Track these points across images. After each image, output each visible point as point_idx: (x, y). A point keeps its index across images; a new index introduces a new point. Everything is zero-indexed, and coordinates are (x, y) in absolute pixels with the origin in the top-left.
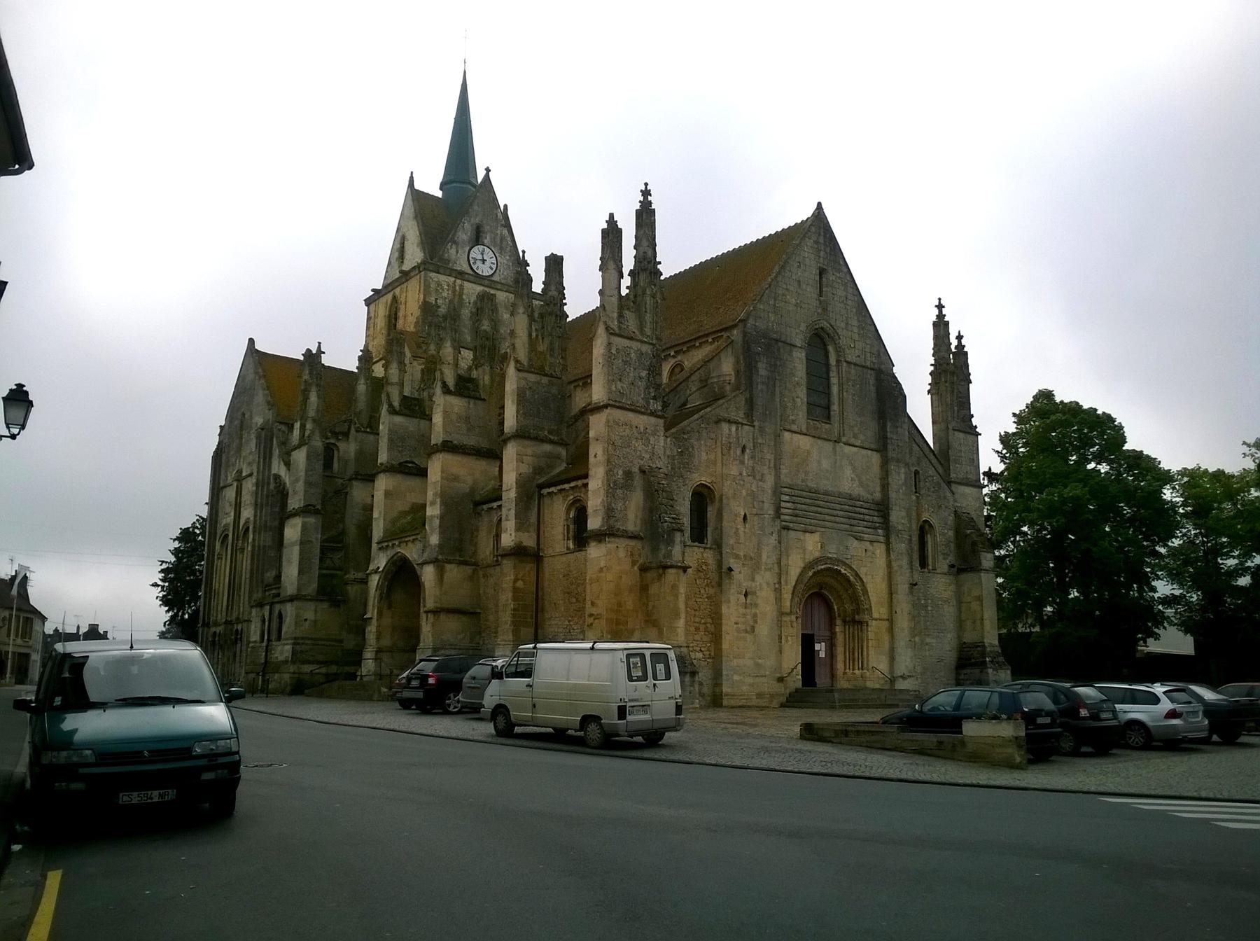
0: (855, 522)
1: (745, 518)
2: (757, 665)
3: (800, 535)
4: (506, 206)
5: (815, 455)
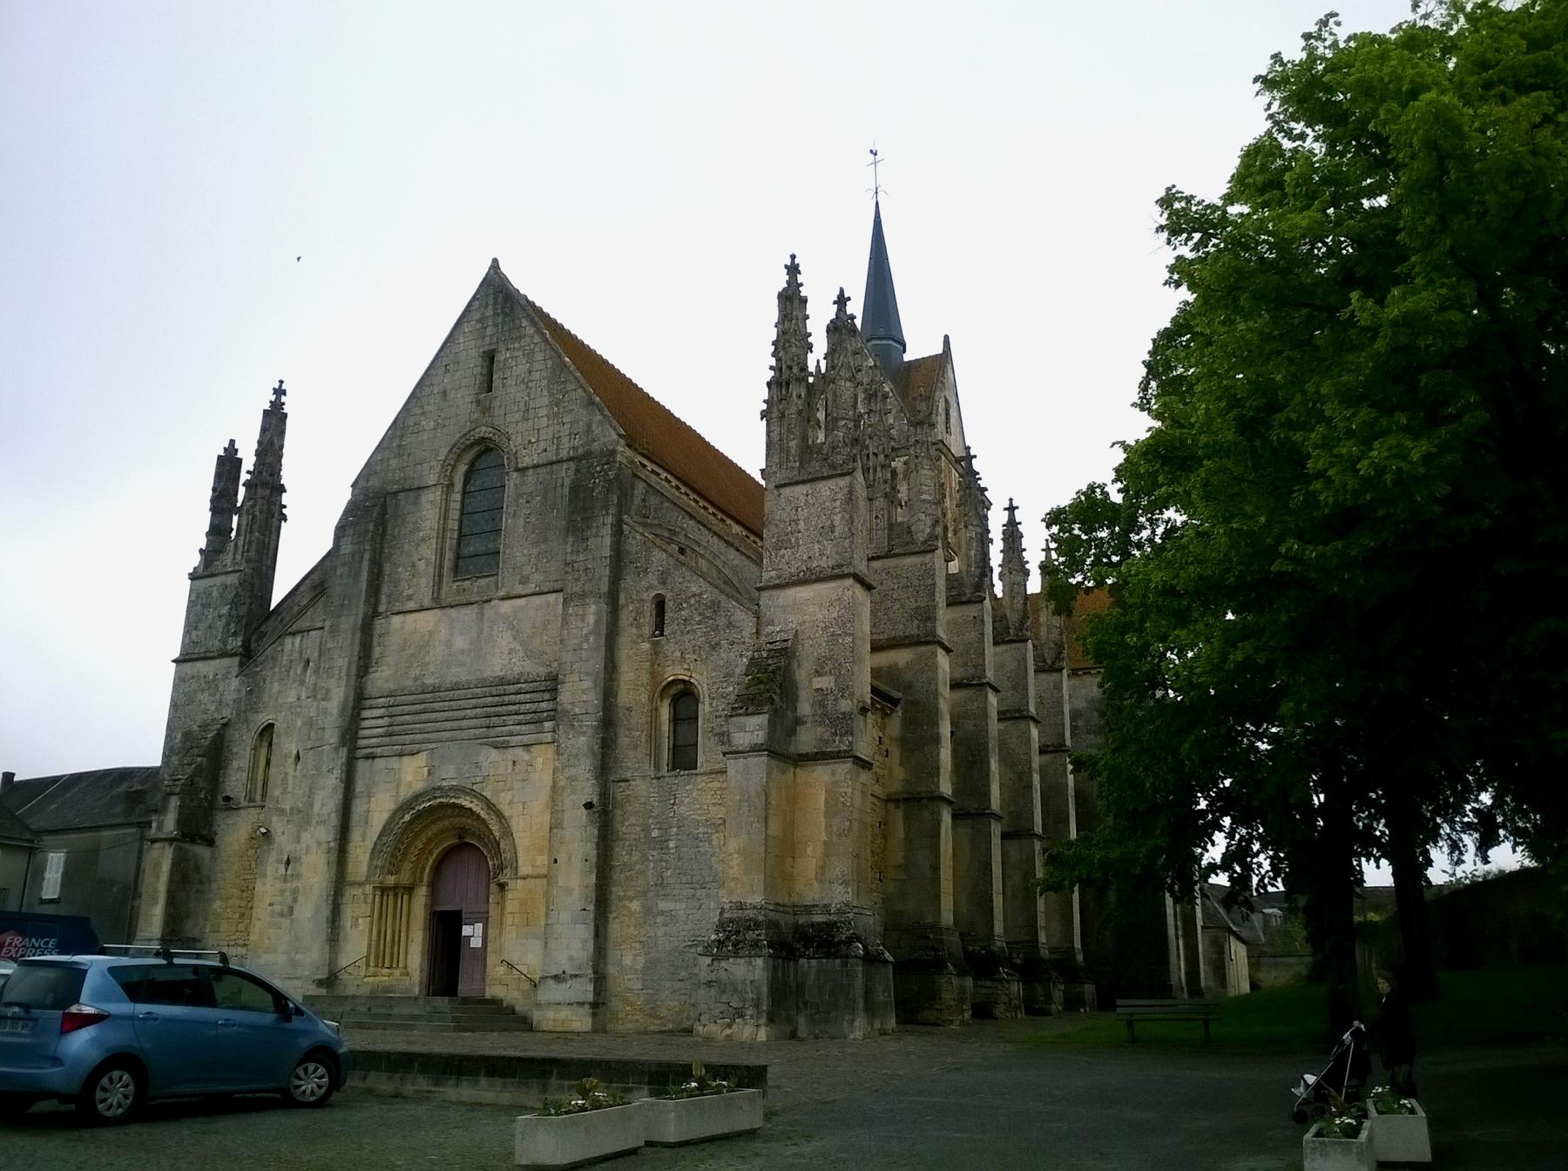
1: (298, 758)
5: (443, 634)
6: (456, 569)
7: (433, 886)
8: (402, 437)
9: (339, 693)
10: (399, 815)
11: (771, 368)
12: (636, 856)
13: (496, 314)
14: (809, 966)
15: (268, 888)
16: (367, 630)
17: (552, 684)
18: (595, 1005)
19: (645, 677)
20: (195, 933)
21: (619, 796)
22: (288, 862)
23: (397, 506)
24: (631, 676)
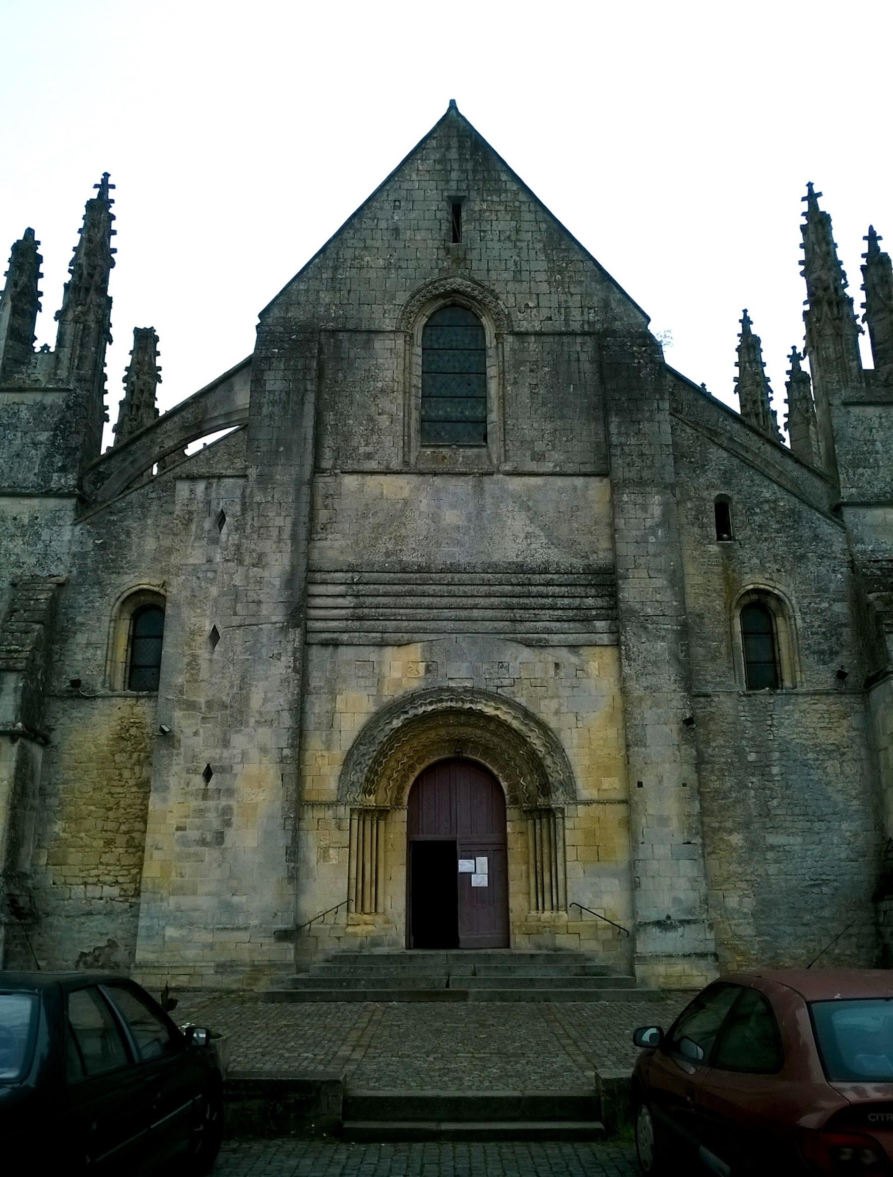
0: (519, 613)
1: (215, 636)
2: (228, 908)
3: (371, 654)
5: (424, 504)
6: (422, 431)
9: (279, 563)
19: (717, 583)
22: (208, 774)
24: (699, 580)
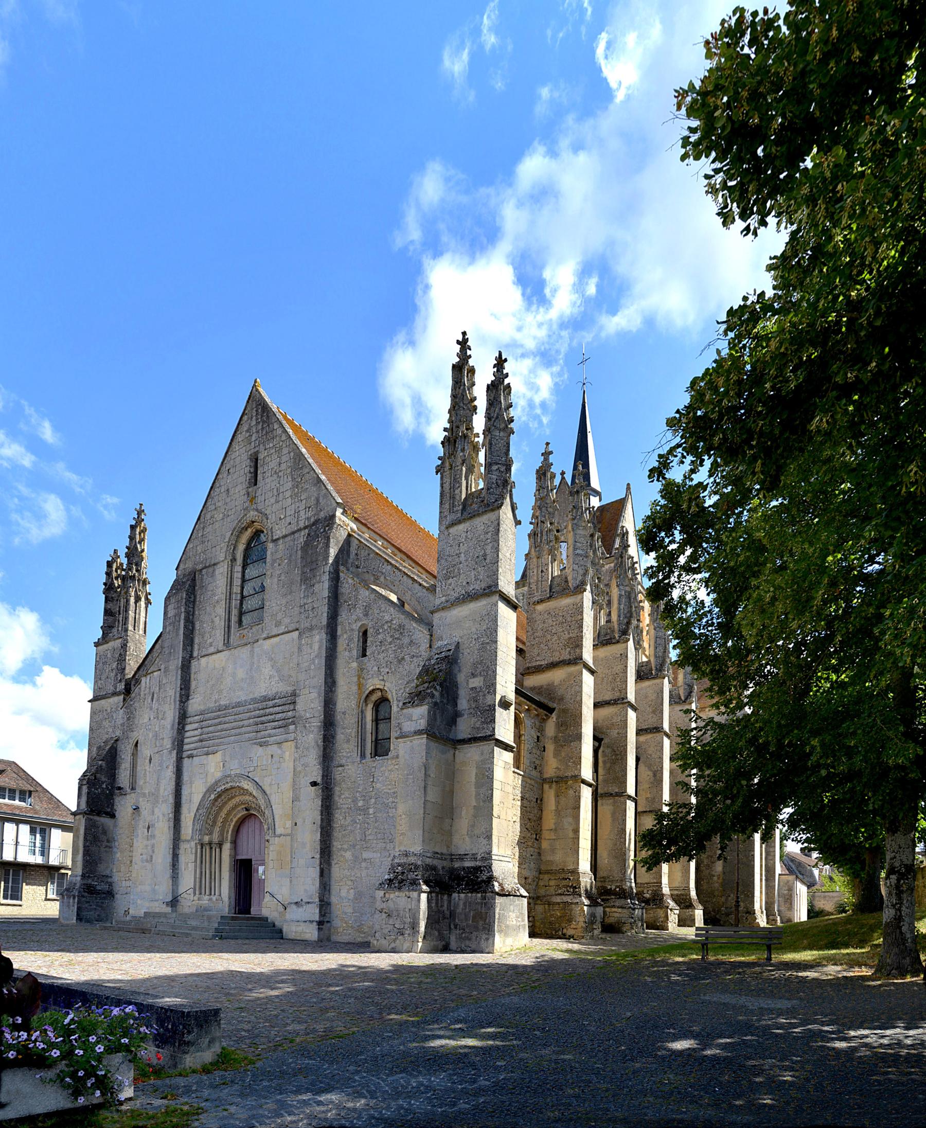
4: (771, 258)
6: (240, 622)
7: (234, 842)
8: (203, 528)
9: (170, 714)
10: (207, 795)
11: (445, 430)
12: (349, 819)
13: (258, 423)
14: (460, 898)
15: (140, 844)
16: (186, 668)
17: (292, 699)
18: (320, 923)
19: (355, 688)
20: (108, 872)
21: (338, 777)
22: (149, 827)
23: (202, 579)
